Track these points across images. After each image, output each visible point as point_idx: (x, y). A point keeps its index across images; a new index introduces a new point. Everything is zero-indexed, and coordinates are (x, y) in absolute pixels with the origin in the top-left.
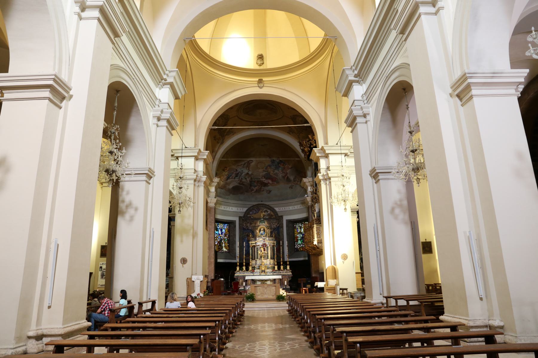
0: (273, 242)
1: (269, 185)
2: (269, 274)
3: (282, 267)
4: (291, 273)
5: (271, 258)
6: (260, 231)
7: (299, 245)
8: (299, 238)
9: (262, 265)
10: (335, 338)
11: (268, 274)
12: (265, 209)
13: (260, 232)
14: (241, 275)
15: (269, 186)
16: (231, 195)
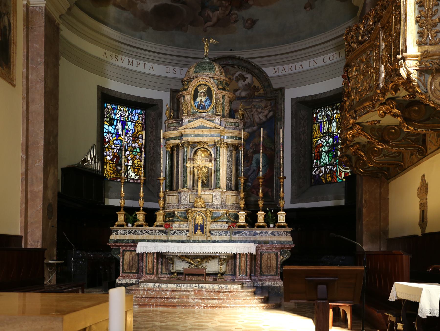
0: (235, 133)
2: (218, 238)
3: (261, 217)
4: (289, 238)
5: (229, 188)
6: (196, 95)
7: (322, 167)
8: (324, 149)
9: (194, 207)
11: (213, 238)
12: (239, 73)
13: (195, 100)
15: (251, 6)
16: (150, 30)
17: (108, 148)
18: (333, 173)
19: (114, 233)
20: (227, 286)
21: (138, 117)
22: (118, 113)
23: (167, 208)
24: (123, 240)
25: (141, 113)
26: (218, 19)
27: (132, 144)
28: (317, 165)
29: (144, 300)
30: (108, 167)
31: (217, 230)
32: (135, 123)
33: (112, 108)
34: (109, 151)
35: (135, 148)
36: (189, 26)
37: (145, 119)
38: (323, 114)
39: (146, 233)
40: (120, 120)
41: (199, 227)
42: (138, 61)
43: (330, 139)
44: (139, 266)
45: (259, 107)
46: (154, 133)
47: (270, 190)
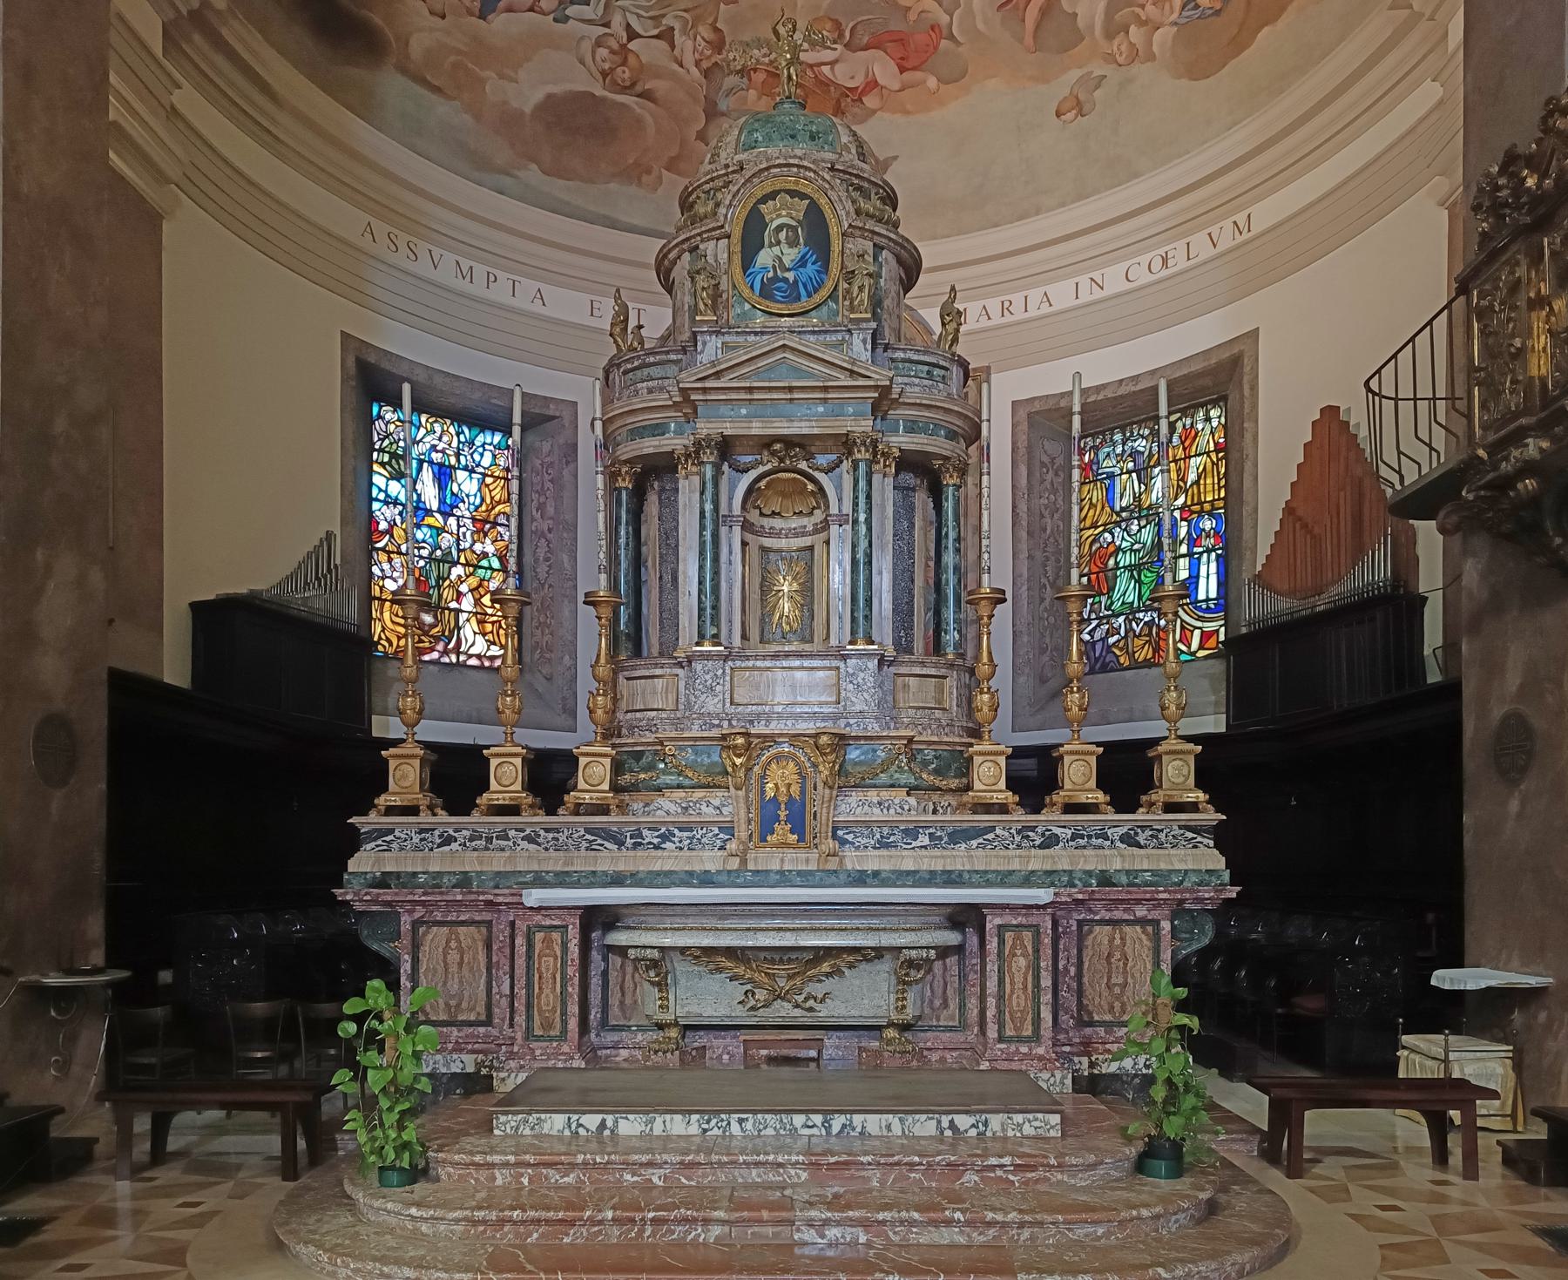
1: (870, 101)
6: (753, 236)
8: (1125, 560)
10: (645, 653)
13: (747, 262)
14: (437, 862)
17: (389, 553)
18: (1158, 634)
19: (373, 845)
20: (986, 1124)
21: (494, 456)
22: (421, 441)
23: (624, 731)
24: (415, 874)
25: (503, 444)
27: (474, 542)
29: (517, 1235)
30: (387, 615)
31: (867, 824)
32: (485, 475)
33: (399, 420)
34: (390, 560)
35: (485, 555)
38: (1119, 450)
39: (524, 844)
40: (431, 462)
42: (490, 270)
43: (1145, 527)
44: (495, 990)
46: (550, 510)
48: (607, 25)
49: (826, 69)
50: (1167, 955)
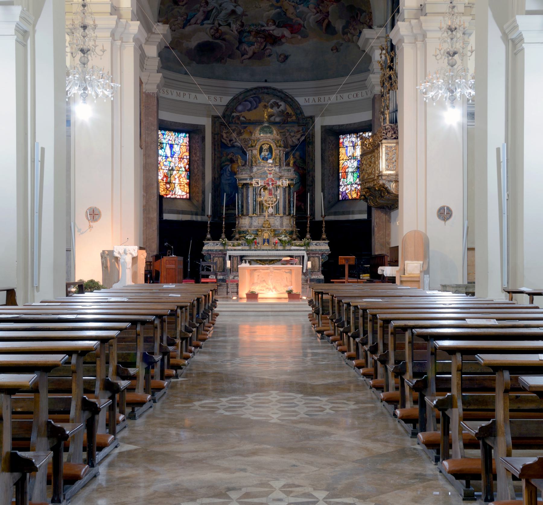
4: (328, 248)
8: (350, 170)
15: (284, 43)
26: (254, 53)
28: (344, 183)
32: (181, 145)
36: (228, 59)
37: (189, 142)
38: (349, 140)
40: (169, 144)
41: (266, 241)
45: (292, 131)
47: (303, 204)
48: (213, 24)
49: (271, 32)
50: (321, 262)
